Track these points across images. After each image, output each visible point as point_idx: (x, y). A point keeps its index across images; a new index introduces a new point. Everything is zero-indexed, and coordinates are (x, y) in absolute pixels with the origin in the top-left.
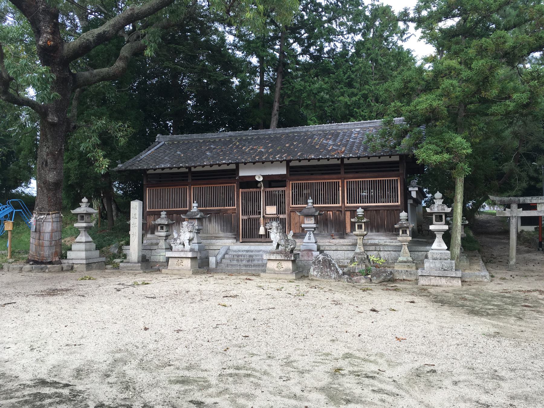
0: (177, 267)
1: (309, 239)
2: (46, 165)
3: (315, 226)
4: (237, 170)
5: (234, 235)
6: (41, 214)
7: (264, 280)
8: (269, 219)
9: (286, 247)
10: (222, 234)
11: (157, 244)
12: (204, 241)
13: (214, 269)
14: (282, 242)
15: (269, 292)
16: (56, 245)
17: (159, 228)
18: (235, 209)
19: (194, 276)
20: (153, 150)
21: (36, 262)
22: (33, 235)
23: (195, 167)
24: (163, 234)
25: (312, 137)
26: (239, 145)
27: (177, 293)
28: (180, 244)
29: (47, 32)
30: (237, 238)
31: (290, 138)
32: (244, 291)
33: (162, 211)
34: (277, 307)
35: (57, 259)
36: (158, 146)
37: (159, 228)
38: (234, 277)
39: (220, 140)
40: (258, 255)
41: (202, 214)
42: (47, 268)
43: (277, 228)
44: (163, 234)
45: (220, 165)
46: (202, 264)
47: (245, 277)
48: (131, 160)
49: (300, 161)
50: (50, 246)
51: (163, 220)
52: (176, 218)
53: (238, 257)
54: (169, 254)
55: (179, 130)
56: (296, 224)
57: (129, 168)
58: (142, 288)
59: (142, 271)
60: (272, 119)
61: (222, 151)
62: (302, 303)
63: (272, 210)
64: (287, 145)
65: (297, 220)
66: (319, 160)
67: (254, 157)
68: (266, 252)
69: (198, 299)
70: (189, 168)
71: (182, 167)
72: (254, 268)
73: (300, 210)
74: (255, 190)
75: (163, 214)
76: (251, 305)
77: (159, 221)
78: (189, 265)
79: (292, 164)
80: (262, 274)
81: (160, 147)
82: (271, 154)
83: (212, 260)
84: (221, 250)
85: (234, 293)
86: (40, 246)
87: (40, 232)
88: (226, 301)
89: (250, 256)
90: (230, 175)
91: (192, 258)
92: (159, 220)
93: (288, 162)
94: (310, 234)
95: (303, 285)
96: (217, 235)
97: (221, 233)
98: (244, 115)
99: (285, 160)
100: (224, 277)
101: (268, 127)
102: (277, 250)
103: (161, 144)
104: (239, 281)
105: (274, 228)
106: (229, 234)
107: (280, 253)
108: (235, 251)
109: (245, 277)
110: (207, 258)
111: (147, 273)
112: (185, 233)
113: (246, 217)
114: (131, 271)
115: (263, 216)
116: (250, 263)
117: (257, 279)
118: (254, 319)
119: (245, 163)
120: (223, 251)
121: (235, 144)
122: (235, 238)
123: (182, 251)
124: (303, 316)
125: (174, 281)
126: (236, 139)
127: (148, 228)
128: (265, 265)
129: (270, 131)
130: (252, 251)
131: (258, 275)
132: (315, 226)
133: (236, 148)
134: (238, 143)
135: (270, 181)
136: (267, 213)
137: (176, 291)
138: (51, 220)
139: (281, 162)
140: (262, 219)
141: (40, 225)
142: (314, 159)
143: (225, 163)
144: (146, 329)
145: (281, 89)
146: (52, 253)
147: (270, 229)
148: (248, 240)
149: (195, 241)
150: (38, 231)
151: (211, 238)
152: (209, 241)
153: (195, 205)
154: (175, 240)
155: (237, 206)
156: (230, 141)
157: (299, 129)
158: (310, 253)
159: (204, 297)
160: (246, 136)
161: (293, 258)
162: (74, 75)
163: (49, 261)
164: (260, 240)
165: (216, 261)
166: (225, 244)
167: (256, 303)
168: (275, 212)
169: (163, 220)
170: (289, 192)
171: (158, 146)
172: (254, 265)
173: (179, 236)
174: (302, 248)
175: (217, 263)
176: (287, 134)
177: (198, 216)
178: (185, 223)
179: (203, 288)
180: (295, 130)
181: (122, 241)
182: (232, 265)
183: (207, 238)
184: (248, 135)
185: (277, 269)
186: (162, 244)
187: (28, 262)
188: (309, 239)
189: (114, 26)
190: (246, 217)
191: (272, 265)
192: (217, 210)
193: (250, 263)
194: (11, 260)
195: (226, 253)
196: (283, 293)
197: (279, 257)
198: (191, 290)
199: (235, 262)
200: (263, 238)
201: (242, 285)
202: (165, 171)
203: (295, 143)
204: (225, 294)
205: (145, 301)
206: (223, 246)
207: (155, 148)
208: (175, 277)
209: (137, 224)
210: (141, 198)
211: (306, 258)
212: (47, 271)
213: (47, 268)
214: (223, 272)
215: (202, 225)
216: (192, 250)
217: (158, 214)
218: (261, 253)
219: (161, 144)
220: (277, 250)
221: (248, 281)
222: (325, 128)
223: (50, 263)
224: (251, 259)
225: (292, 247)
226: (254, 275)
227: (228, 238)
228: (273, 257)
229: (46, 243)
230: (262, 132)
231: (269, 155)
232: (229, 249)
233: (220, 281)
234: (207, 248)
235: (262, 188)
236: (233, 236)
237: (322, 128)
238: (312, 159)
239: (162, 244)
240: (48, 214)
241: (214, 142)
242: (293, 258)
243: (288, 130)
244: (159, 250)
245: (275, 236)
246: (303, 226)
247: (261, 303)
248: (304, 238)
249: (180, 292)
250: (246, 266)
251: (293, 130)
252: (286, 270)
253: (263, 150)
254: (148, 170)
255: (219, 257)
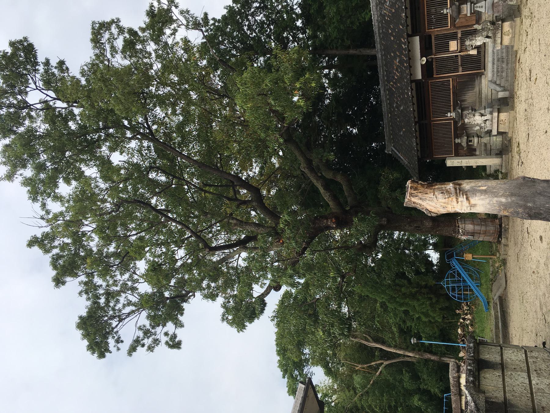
0: (507, 124)
1: (482, 7)
2: (419, 227)
3: (469, 4)
4: (417, 82)
5: (477, 78)
6: (459, 232)
7: (520, 47)
8: (462, 47)
9: (489, 29)
10: (477, 89)
11: (486, 145)
12: (483, 104)
13: (510, 93)
14: (485, 33)
15: (528, 43)
16: (485, 222)
17: (470, 143)
18: (452, 79)
19: (515, 109)
20: (399, 155)
21: (500, 236)
22: (476, 238)
23: (415, 118)
24: (476, 140)
25: (382, 16)
26: (393, 82)
27: (527, 118)
28: (485, 123)
29: (327, 222)
30: (482, 74)
31: (385, 36)
32: (527, 65)
33: (455, 142)
34: (539, 37)
35: (497, 221)
36: (396, 151)
37: (470, 143)
38: (517, 73)
39: (388, 99)
40: (498, 53)
41: (457, 108)
42: (505, 227)
43: (471, 40)
44: (476, 140)
45: (413, 97)
46: (505, 103)
47: (518, 64)
48: (409, 170)
49: (408, 26)
50: (486, 226)
51: (463, 141)
52: (462, 129)
53: (499, 72)
54: (495, 132)
55: (380, 137)
56: (467, 20)
57: (417, 171)
58: (522, 146)
59: (510, 154)
60: (364, 54)
61: (399, 96)
62: (537, 16)
63: (453, 45)
64: (392, 38)
65: (463, 20)
66: (406, 8)
67: (405, 67)
68: (494, 47)
69: (531, 100)
70: (416, 123)
71: (415, 128)
72: (509, 58)
73: (453, 20)
74: (434, 63)
75: (458, 141)
76: (537, 58)
77: (464, 144)
78: (505, 114)
79: (410, 33)
80: (515, 49)
81: (396, 149)
82: (402, 53)
83: (501, 95)
84: (492, 88)
85: (528, 72)
86: (485, 233)
87: (474, 233)
88: (533, 79)
89: (498, 61)
90: (420, 86)
91: (499, 112)
92: (463, 144)
93: (409, 36)
94: (477, 7)
95: (525, 12)
96: (478, 92)
97: (475, 90)
98: (361, 79)
99: (407, 39)
100: (517, 83)
101: (374, 57)
102: (492, 37)
103: (394, 149)
104: (520, 69)
105: (471, 43)
106: (477, 82)
107: (495, 35)
108: (493, 75)
109: (518, 64)
110: (500, 100)
111: (512, 149)
112: (476, 120)
113: (460, 69)
114: (509, 163)
115: (459, 52)
116: (505, 60)
117: (519, 52)
118: (545, 56)
119: (411, 75)
120: (493, 86)
121: (392, 86)
122: (481, 76)
123: (492, 121)
124: (545, 16)
125: (518, 123)
126: (387, 85)
127: (471, 152)
128: (507, 47)
129: (379, 56)
130: (494, 59)
131: (516, 51)
132: (469, 4)
133: (396, 84)
134: (391, 83)
135: (426, 50)
136: (456, 49)
137: (525, 120)
138: (463, 225)
139: (409, 43)
140: (462, 54)
141: (468, 233)
142: (406, 13)
143: (411, 93)
144: (546, 132)
145: (337, 48)
146: (493, 224)
147: (472, 46)
148: (482, 64)
149: (483, 112)
150: (473, 234)
151: (480, 98)
152: (483, 99)
153: (449, 115)
154: (481, 128)
155: (450, 78)
156: (390, 90)
157: (376, 29)
158: (495, 5)
159: (530, 96)
160: (383, 77)
161: (500, 22)
162: (351, 208)
163: (498, 227)
164: (482, 53)
165: (502, 91)
166: (486, 85)
167: (535, 54)
168: (456, 42)
169: (463, 141)
170: (436, 31)
171: (396, 151)
172: (507, 56)
173: (478, 125)
174: (490, 13)
175: (505, 90)
176: (380, 39)
177: (460, 111)
178: (466, 121)
179: (523, 99)
180: (377, 32)
181: (482, 175)
182: (507, 76)
183: (480, 102)
184: (383, 74)
185: (510, 36)
186: (485, 140)
187: (499, 242)
188: (482, 7)
189: (317, 180)
190: (460, 69)
191: (507, 40)
192: (453, 95)
193: (505, 60)
194: (498, 255)
195: (495, 83)
196: (529, 31)
197: (499, 35)
198: (524, 108)
199: (504, 74)
200: (480, 50)
201: (522, 66)
202: (418, 142)
203: (390, 31)
204: (528, 80)
205: (531, 140)
206: (488, 86)
207: (397, 153)
208: (515, 125)
209: (467, 160)
210: (444, 160)
211: (501, 8)
212: (507, 227)
213: (505, 227)
214: (512, 85)
215: (468, 107)
216: (491, 113)
217: (458, 145)
218: (495, 51)
219: (394, 149)
220: (492, 37)
221: (520, 61)
222: (374, 4)
223: (501, 225)
224: (501, 60)
225: (489, 24)
226: (516, 56)
227: (480, 83)
228: (499, 41)
229: (483, 228)
230: (379, 63)
231: (403, 54)
232: (491, 81)
233: (519, 85)
234: (490, 101)
235: (433, 56)
236: (479, 78)
237: (374, 8)
238: (406, 15)
239: (485, 140)
240: (459, 227)
241: (391, 104)
242: (500, 22)
243: (377, 38)
244: (491, 142)
245: (479, 41)
246: (469, 15)
247: (536, 50)
248: (481, 12)
249: (526, 116)
250: (508, 63)
251: (377, 34)
252: (511, 27)
253: (398, 60)
254: (418, 156)
255: (498, 89)
